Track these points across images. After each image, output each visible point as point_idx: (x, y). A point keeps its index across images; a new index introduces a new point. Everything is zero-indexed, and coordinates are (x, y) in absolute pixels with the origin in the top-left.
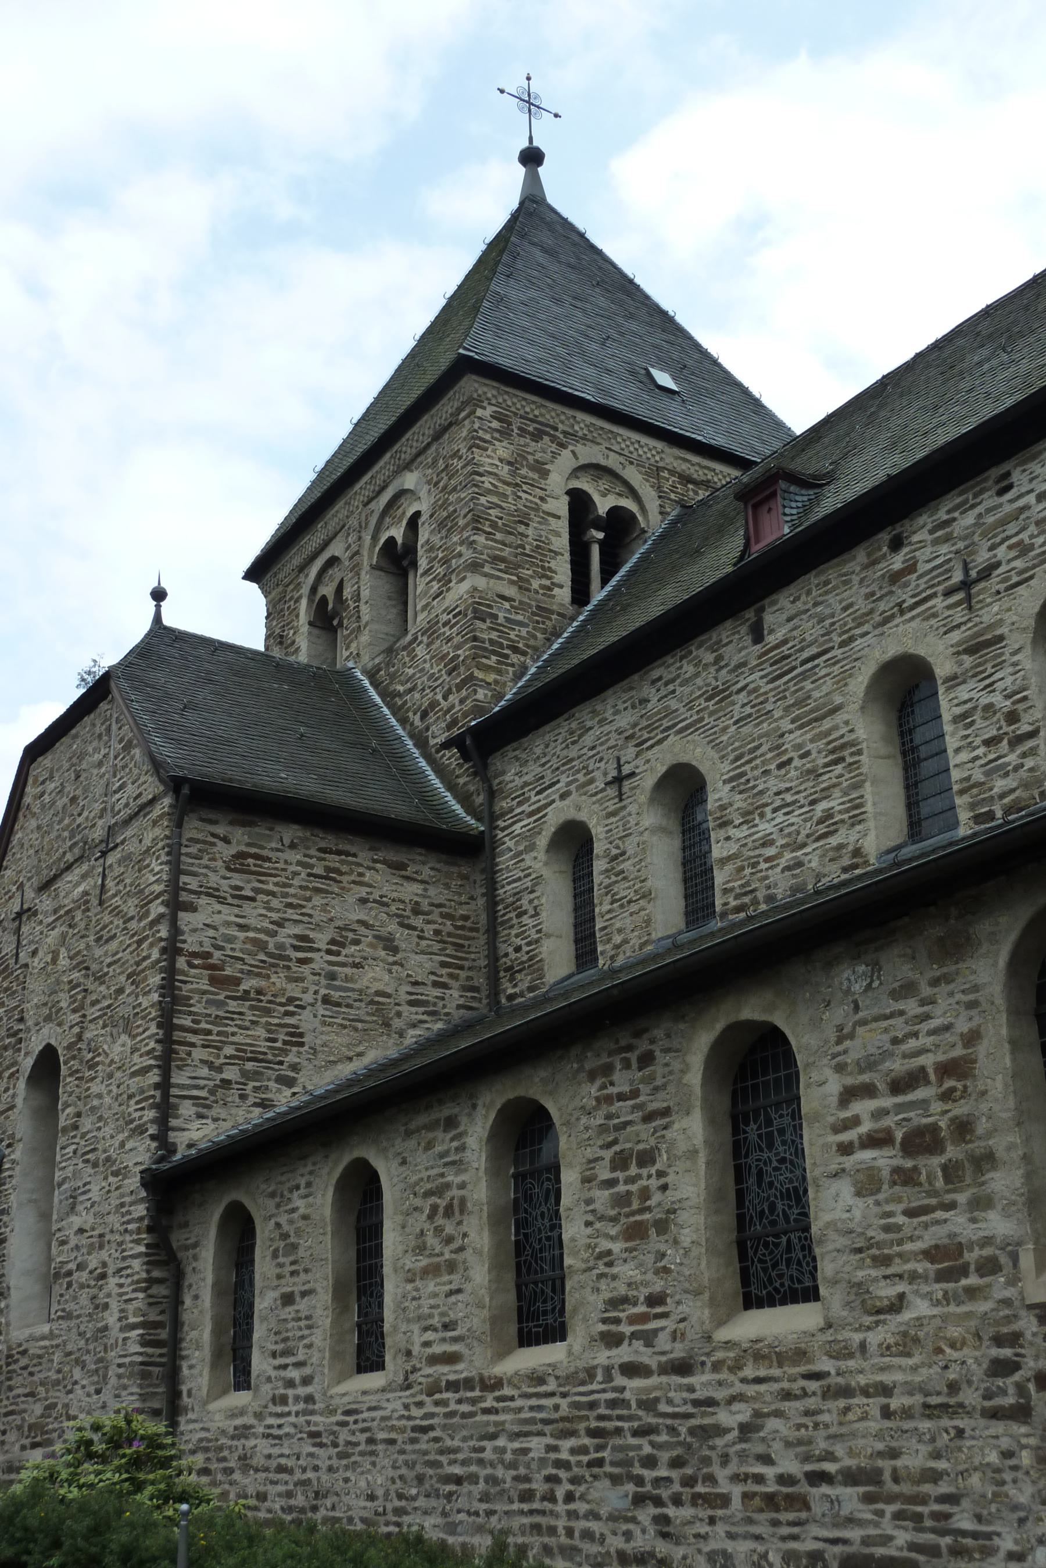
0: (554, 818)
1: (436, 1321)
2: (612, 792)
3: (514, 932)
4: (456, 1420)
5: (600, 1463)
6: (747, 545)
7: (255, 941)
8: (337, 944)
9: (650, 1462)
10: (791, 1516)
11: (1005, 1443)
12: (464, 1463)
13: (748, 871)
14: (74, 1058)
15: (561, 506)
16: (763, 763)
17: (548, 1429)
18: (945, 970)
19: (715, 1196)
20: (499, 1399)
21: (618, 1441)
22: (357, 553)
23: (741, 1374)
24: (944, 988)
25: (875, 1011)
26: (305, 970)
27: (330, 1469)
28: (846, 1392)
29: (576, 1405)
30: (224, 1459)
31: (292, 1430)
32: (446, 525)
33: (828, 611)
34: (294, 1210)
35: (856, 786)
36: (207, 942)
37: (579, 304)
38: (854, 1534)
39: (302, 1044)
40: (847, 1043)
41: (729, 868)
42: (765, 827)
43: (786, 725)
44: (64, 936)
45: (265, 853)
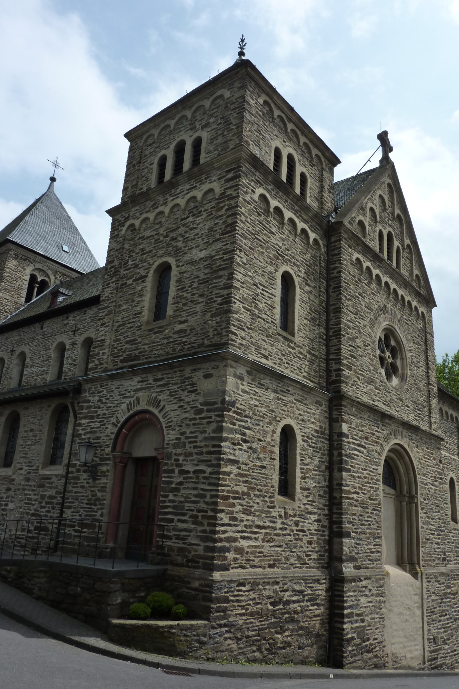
15: (28, 278)
42: (33, 370)
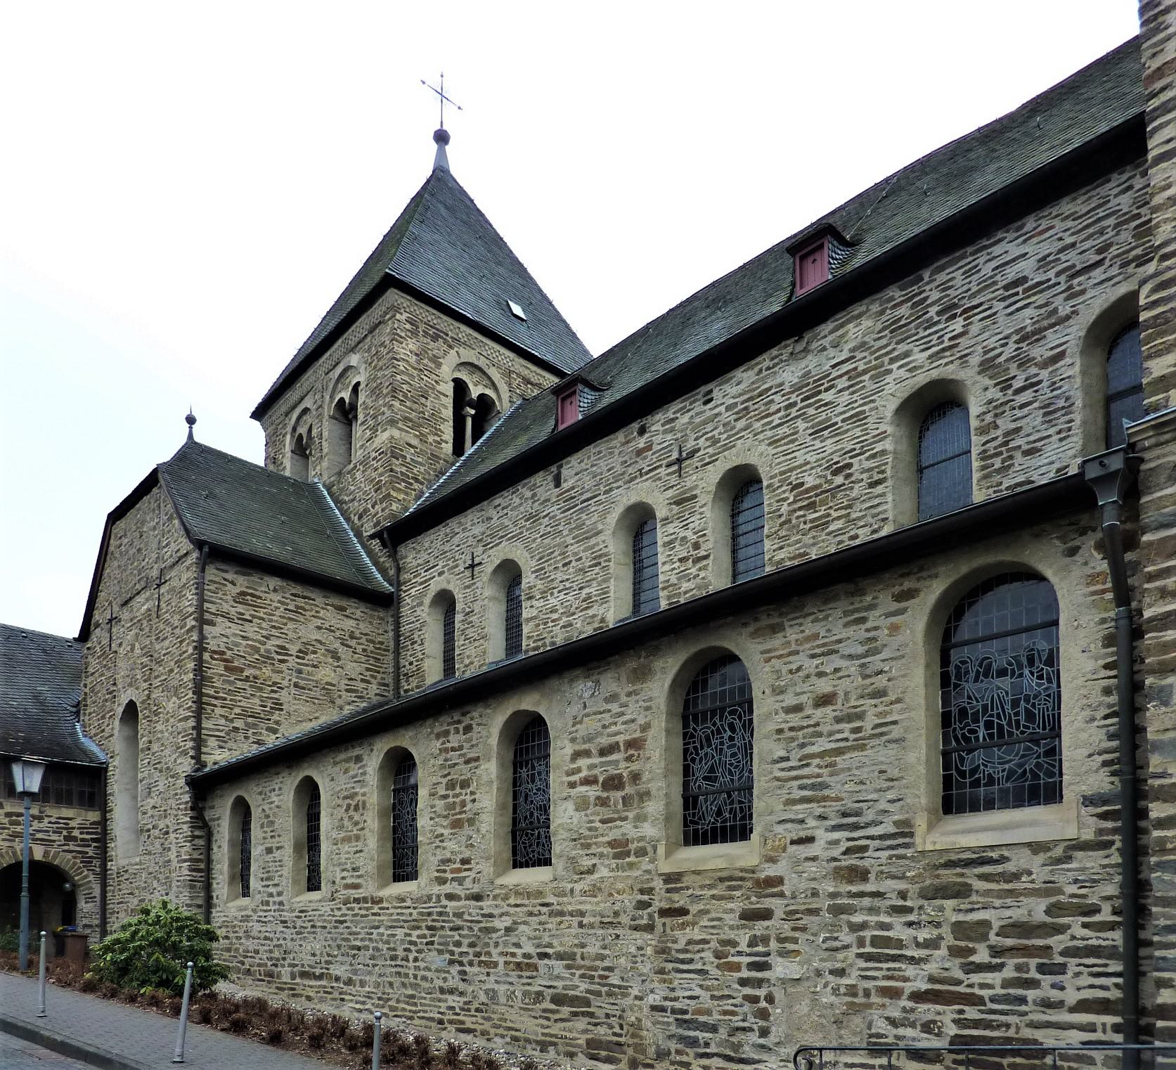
0: (436, 585)
1: (348, 866)
2: (468, 573)
3: (409, 653)
4: (358, 918)
5: (432, 943)
6: (556, 425)
7: (252, 647)
8: (302, 653)
9: (458, 944)
10: (528, 974)
11: (639, 943)
12: (362, 940)
13: (542, 627)
14: (146, 709)
15: (449, 389)
16: (555, 562)
17: (406, 925)
18: (635, 688)
19: (501, 807)
20: (381, 909)
21: (442, 933)
22: (320, 406)
23: (508, 902)
24: (634, 698)
25: (595, 709)
26: (283, 666)
27: (292, 939)
28: (561, 914)
29: (421, 914)
30: (236, 932)
31: (272, 919)
32: (375, 392)
33: (599, 471)
34: (272, 803)
35: (605, 581)
36: (222, 645)
37: (467, 250)
38: (559, 984)
39: (282, 710)
40: (578, 726)
41: (531, 624)
42: (553, 601)
43: (569, 540)
44: (137, 635)
45: (257, 593)
